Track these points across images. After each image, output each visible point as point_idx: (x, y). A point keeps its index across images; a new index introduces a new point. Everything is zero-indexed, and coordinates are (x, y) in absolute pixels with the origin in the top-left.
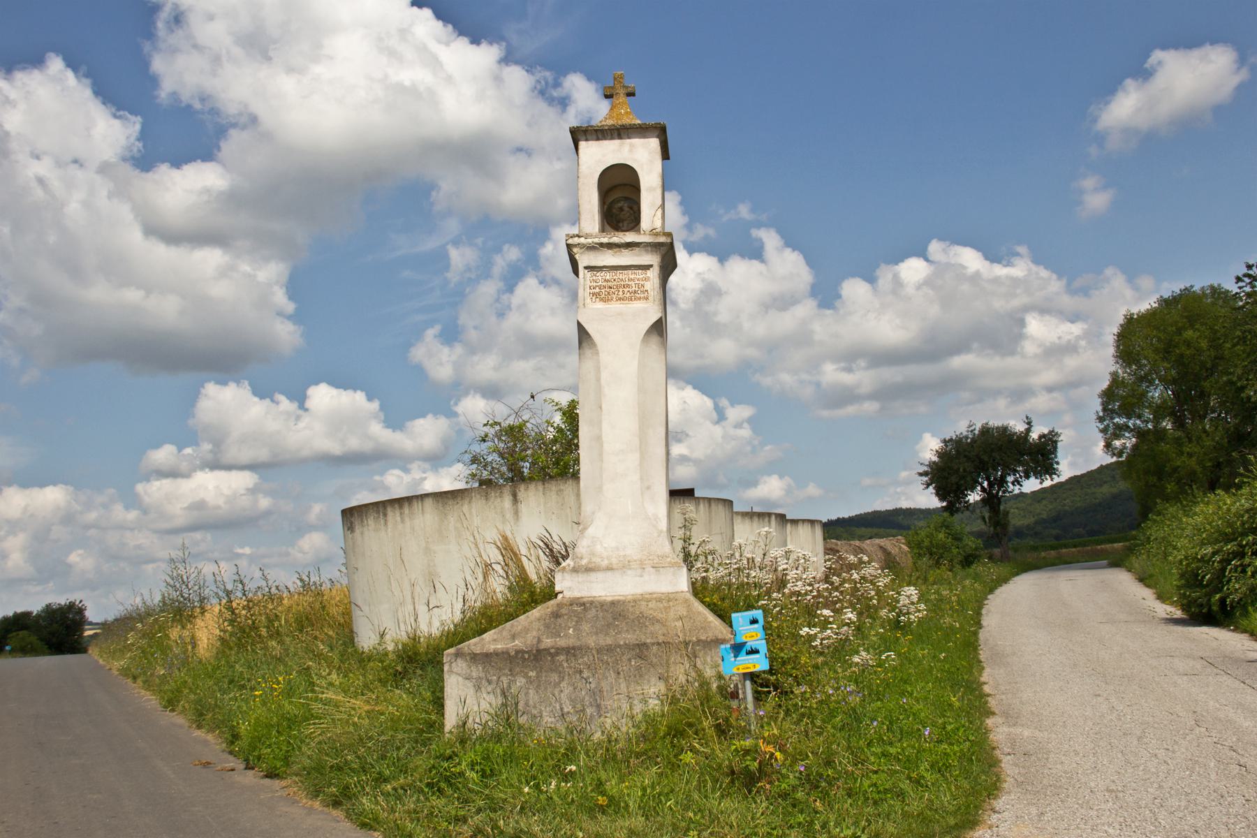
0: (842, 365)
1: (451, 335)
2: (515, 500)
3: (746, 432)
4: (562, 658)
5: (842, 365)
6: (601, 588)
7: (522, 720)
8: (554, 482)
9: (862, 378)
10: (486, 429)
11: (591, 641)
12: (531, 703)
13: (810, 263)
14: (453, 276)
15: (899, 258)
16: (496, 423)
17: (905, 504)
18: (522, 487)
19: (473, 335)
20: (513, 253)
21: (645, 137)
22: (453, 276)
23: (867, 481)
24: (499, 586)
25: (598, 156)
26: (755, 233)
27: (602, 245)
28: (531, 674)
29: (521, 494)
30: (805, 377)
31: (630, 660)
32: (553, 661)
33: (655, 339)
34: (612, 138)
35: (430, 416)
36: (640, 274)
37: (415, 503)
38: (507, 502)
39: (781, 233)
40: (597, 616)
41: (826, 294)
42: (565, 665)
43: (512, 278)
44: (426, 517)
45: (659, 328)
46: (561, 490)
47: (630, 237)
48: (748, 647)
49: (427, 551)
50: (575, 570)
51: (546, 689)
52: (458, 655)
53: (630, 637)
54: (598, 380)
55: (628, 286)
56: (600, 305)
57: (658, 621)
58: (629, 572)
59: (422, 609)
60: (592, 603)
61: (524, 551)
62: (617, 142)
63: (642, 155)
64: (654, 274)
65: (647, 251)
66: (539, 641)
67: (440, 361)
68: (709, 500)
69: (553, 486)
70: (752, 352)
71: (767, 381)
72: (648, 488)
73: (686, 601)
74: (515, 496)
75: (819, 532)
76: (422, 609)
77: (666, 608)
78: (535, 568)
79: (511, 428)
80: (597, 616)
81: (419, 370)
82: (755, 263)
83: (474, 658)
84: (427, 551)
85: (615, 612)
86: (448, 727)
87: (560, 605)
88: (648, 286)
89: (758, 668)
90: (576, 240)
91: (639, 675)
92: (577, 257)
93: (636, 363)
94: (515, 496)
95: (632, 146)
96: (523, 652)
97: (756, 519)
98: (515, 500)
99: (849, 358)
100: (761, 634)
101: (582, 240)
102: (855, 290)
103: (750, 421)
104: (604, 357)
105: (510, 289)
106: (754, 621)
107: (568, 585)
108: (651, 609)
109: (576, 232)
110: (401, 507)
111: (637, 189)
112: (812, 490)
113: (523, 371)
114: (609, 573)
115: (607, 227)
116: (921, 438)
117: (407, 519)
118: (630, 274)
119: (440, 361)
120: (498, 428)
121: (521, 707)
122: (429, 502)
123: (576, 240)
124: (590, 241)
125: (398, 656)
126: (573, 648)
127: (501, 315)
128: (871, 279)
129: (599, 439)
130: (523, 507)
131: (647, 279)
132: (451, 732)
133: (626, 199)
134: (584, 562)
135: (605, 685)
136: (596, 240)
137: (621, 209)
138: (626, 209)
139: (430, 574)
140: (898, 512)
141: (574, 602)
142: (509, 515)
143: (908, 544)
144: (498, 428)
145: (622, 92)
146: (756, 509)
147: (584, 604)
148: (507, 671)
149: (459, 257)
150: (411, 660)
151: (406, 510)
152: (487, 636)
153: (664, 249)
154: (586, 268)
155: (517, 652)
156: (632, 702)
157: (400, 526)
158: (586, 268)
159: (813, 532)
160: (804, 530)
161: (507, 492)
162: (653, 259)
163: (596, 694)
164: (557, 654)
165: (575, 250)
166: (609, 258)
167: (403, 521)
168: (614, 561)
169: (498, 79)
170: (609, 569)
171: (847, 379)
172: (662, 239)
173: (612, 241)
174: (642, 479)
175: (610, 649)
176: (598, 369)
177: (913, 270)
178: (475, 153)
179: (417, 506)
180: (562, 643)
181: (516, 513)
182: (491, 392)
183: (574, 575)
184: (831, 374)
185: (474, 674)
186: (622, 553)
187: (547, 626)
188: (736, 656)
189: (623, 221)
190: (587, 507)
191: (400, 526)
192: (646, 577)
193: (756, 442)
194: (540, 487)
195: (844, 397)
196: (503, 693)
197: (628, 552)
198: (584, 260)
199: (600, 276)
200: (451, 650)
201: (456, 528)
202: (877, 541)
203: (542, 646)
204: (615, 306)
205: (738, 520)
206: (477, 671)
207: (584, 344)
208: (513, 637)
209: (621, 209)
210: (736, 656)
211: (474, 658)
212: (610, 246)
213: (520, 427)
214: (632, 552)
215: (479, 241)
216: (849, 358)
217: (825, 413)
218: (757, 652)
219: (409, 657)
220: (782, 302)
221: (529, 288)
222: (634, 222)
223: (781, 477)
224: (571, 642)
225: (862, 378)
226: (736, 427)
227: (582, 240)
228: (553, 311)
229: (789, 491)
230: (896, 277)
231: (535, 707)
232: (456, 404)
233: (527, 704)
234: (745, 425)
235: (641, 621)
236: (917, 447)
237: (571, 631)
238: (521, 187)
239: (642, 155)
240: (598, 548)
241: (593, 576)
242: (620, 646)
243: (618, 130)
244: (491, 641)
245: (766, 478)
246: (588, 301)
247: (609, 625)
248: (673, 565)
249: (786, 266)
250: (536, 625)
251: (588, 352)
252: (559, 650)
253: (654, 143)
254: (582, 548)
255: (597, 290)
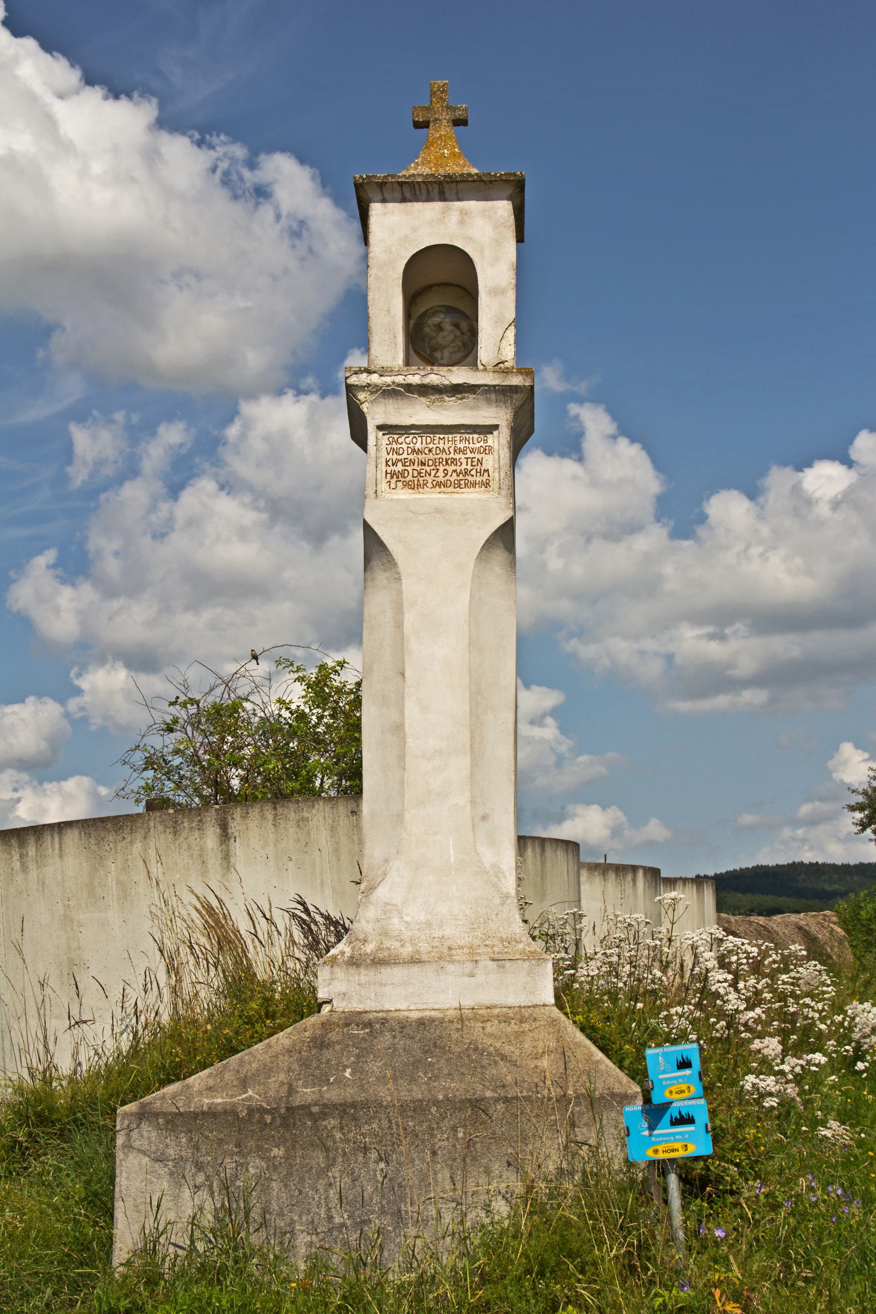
0: (710, 629)
1: (75, 566)
2: (225, 835)
3: (549, 732)
4: (332, 1122)
5: (710, 629)
6: (399, 995)
7: (255, 1239)
8: (292, 806)
9: (744, 651)
10: (175, 710)
11: (384, 1093)
12: (274, 1206)
13: (658, 463)
14: (79, 476)
15: (803, 464)
16: (192, 701)
17: (808, 857)
18: (238, 812)
19: (112, 567)
20: (174, 434)
21: (486, 199)
22: (79, 476)
23: (748, 819)
24: (205, 986)
25: (402, 229)
26: (573, 409)
27: (409, 388)
28: (275, 1151)
29: (235, 826)
30: (649, 645)
31: (454, 1129)
32: (315, 1128)
33: (499, 555)
34: (429, 199)
35: (31, 699)
36: (475, 441)
37: (47, 838)
38: (211, 838)
39: (613, 413)
40: (393, 1047)
41: (682, 515)
42: (338, 1136)
43: (178, 478)
44: (68, 862)
45: (505, 535)
46: (305, 820)
47: (459, 376)
48: (673, 1112)
49: (67, 920)
50: (354, 962)
51: (302, 1180)
52: (142, 1115)
53: (453, 1087)
54: (399, 625)
55: (454, 461)
56: (404, 494)
57: (504, 1057)
58: (451, 968)
59: (57, 1025)
60: (384, 1022)
61: (243, 926)
62: (437, 206)
63: (482, 230)
64: (499, 442)
65: (489, 401)
66: (291, 1091)
67: (58, 608)
68: (543, 841)
69: (290, 812)
70: (564, 607)
71: (586, 651)
72: (484, 818)
73: (553, 1022)
74: (224, 827)
75: (709, 896)
76: (57, 1025)
77: (518, 1034)
78: (271, 956)
79: (218, 711)
80: (393, 1047)
81: (24, 623)
82: (569, 466)
83: (175, 1122)
84: (67, 920)
85: (427, 1038)
86: (121, 1253)
87: (327, 1026)
88: (489, 462)
89: (693, 1150)
90: (364, 379)
91: (468, 1157)
92: (365, 407)
93: (465, 597)
94: (224, 827)
95: (464, 213)
96: (262, 1110)
97: (612, 876)
98: (225, 835)
99: (720, 618)
100: (696, 1088)
101: (375, 378)
102: (729, 509)
103: (555, 713)
104: (410, 586)
105: (175, 490)
106: (684, 1064)
107: (340, 989)
108: (487, 1035)
109: (364, 364)
110: (22, 844)
111: (470, 293)
112: (655, 829)
113: (192, 626)
114: (415, 969)
115: (414, 357)
116: (837, 749)
117: (32, 866)
118: (458, 440)
119: (58, 608)
120: (193, 710)
121: (255, 1214)
122: (72, 837)
123: (364, 379)
124: (388, 380)
125: (18, 1113)
126: (354, 1105)
127: (160, 536)
128: (753, 493)
129: (399, 728)
130: (238, 849)
131: (488, 450)
132: (128, 1264)
133: (449, 310)
134: (369, 948)
135: (409, 1174)
136: (400, 379)
137: (439, 328)
138: (448, 327)
139: (72, 963)
140: (796, 868)
141: (353, 1019)
142: (214, 862)
143: (843, 923)
144: (193, 710)
145: (445, 117)
146: (612, 860)
147: (369, 1024)
148: (231, 1147)
149: (92, 444)
150: (42, 1120)
151: (31, 850)
152: (197, 1080)
153: (518, 398)
154: (380, 428)
155: (251, 1111)
156: (469, 1203)
157: (19, 878)
158: (380, 428)
159: (701, 900)
160: (683, 895)
161: (211, 817)
162: (498, 415)
163: (393, 1188)
164: (324, 1115)
165: (362, 396)
166: (420, 413)
167: (24, 868)
168: (424, 947)
169: (151, 157)
170: (415, 961)
171: (714, 650)
172: (516, 380)
173: (426, 381)
174: (473, 802)
175: (419, 1108)
176: (399, 609)
177: (825, 479)
178: (118, 276)
179: (50, 842)
180: (333, 1095)
181: (226, 856)
182: (142, 661)
183: (352, 970)
184: (692, 642)
185: (171, 1152)
186: (437, 933)
187: (305, 1064)
188: (652, 1128)
189: (442, 348)
190: (375, 851)
191: (19, 878)
192: (480, 977)
193: (563, 748)
194: (269, 814)
195: (716, 679)
196: (226, 1187)
197: (448, 931)
198: (377, 413)
199: (405, 442)
200: (131, 1107)
201: (119, 882)
202: (793, 918)
203: (297, 1101)
204: (431, 496)
205: (584, 875)
206: (176, 1146)
207: (375, 563)
208: (244, 1083)
209: (439, 328)
210: (652, 1128)
211: (175, 1122)
212: (424, 390)
213: (235, 708)
214: (455, 933)
215: (119, 416)
216: (720, 618)
217: (684, 706)
218: (690, 1120)
219: (39, 1115)
220: (620, 529)
221: (202, 493)
222: (466, 350)
223: (604, 807)
224: (349, 1094)
225: (744, 651)
226: (532, 722)
227: (375, 378)
228: (243, 534)
229: (616, 832)
230: (797, 489)
231: (281, 1214)
232: (79, 675)
233: (265, 1211)
234: (549, 721)
235: (476, 1057)
236: (831, 764)
237: (348, 1073)
238: (189, 333)
239: (482, 230)
240: (395, 923)
241: (387, 973)
242: (436, 1103)
243: (440, 183)
244: (201, 1089)
245: (580, 809)
246: (383, 486)
247: (417, 1064)
248: (529, 956)
249: (621, 468)
250: (284, 1061)
251: (381, 576)
252: (328, 1109)
253: (503, 208)
254: (365, 923)
255: (400, 467)
